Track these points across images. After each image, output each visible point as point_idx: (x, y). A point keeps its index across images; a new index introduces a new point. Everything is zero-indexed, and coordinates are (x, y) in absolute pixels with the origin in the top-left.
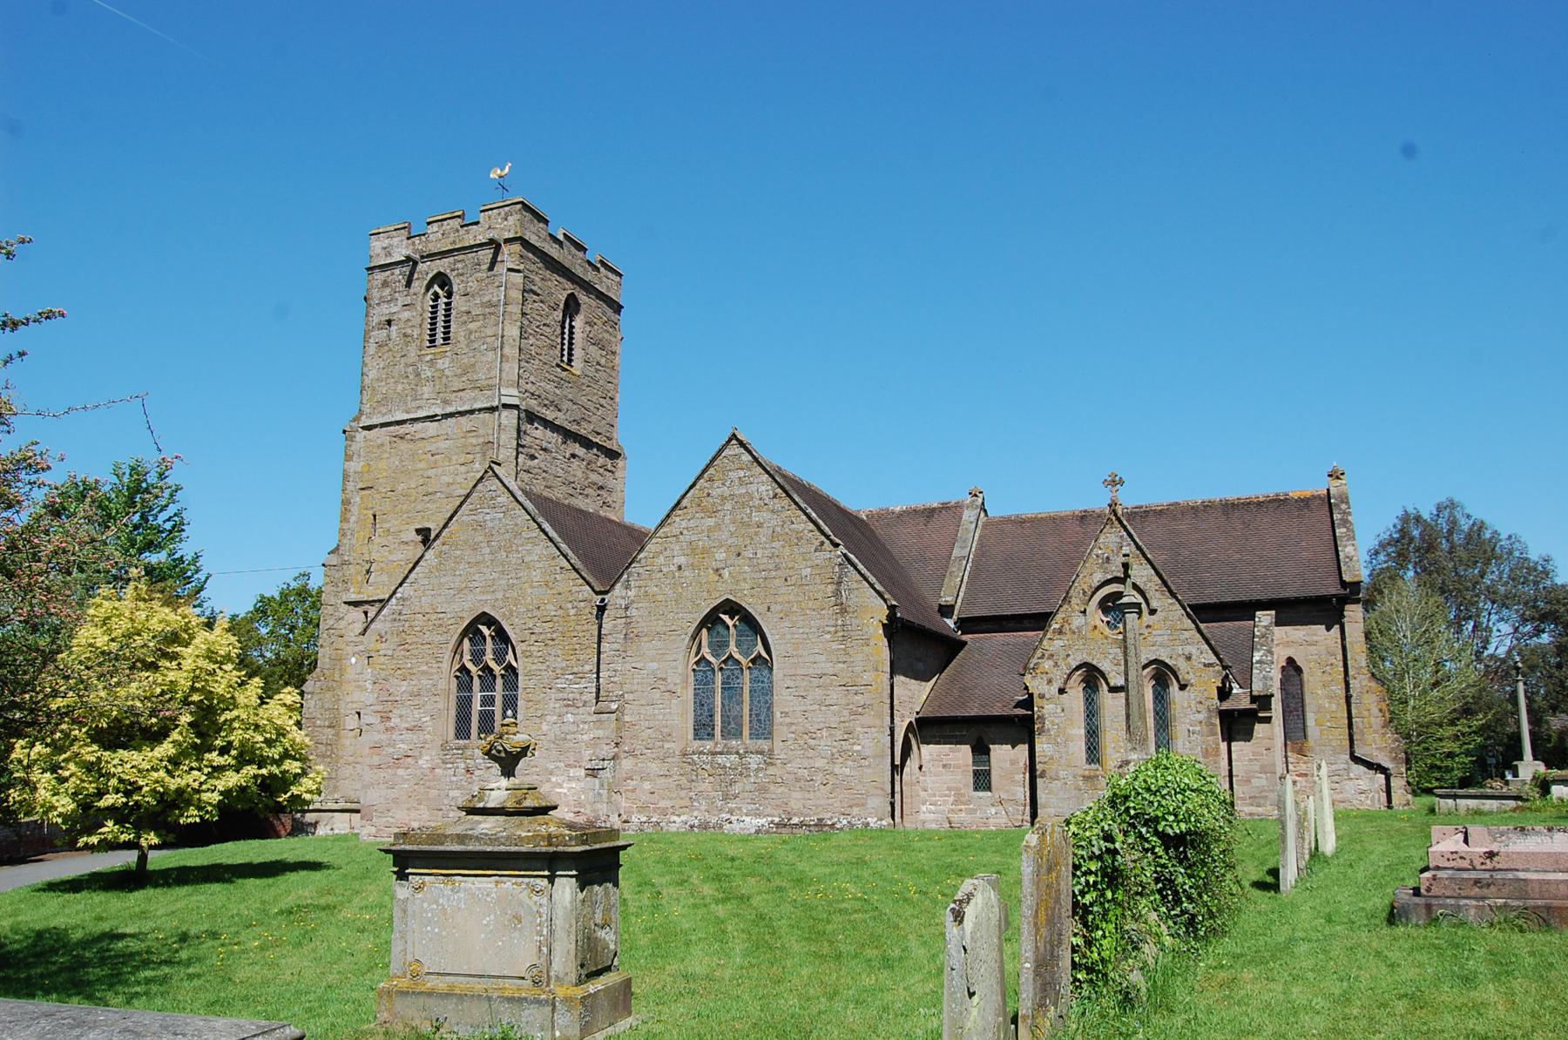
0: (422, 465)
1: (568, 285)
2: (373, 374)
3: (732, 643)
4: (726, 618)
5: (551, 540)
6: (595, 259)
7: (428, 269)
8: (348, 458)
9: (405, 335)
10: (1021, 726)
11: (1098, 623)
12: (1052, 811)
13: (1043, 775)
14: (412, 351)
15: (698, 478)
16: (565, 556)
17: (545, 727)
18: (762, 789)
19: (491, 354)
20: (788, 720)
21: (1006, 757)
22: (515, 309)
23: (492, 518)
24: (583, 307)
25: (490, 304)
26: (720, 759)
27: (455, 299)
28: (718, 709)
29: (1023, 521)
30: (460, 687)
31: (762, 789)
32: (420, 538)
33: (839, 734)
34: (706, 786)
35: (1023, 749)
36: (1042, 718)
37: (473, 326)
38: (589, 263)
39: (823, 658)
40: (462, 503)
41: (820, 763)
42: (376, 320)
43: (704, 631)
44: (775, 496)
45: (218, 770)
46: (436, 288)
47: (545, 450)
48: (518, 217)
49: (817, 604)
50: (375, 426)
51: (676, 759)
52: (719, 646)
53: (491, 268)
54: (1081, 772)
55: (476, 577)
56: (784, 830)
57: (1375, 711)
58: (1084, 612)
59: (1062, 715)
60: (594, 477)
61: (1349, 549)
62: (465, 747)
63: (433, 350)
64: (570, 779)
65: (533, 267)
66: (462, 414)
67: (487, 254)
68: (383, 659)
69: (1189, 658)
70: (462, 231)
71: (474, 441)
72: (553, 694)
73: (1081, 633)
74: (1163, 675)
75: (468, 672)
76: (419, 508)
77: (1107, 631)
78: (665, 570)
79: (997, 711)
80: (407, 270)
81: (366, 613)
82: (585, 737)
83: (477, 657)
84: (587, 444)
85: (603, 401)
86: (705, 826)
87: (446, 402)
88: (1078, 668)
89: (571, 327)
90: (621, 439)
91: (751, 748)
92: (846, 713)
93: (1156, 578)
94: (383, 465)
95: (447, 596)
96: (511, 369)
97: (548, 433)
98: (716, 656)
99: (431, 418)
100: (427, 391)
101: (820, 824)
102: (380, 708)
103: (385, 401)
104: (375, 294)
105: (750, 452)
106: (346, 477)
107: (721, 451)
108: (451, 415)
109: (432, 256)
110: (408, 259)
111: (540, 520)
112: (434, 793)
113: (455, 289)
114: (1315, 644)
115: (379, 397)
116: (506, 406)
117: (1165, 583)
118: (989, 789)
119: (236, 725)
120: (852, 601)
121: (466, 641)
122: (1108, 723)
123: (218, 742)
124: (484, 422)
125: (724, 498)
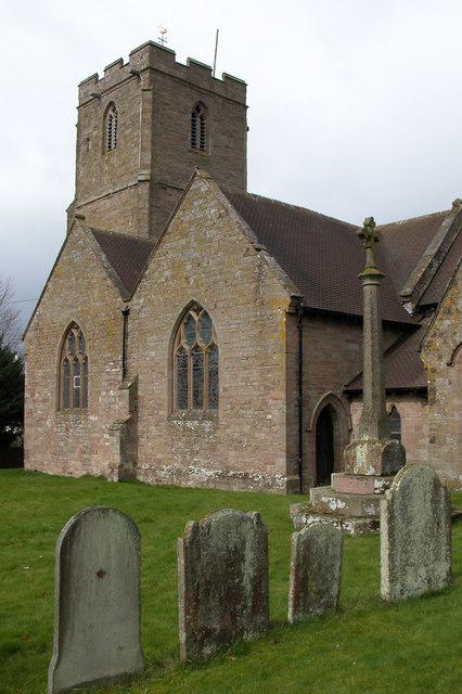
7: (106, 100)
28: (191, 386)
31: (213, 448)
36: (434, 390)
41: (246, 429)
83: (191, 337)
100: (106, 179)
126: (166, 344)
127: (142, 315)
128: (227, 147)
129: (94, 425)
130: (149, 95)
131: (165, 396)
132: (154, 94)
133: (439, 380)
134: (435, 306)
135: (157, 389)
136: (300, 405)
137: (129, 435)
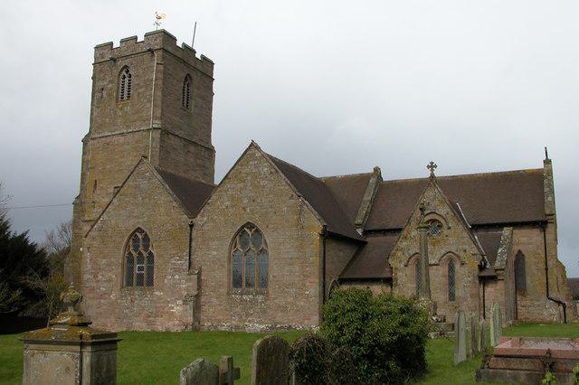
7: (121, 63)
14: (114, 103)
23: (144, 184)
31: (264, 312)
36: (396, 279)
37: (140, 91)
60: (199, 162)
83: (136, 248)
86: (237, 327)
126: (226, 248)
127: (205, 228)
130: (161, 67)
131: (225, 280)
132: (165, 67)
133: (399, 274)
134: (399, 230)
135: (218, 276)
136: (324, 286)
137: (197, 303)
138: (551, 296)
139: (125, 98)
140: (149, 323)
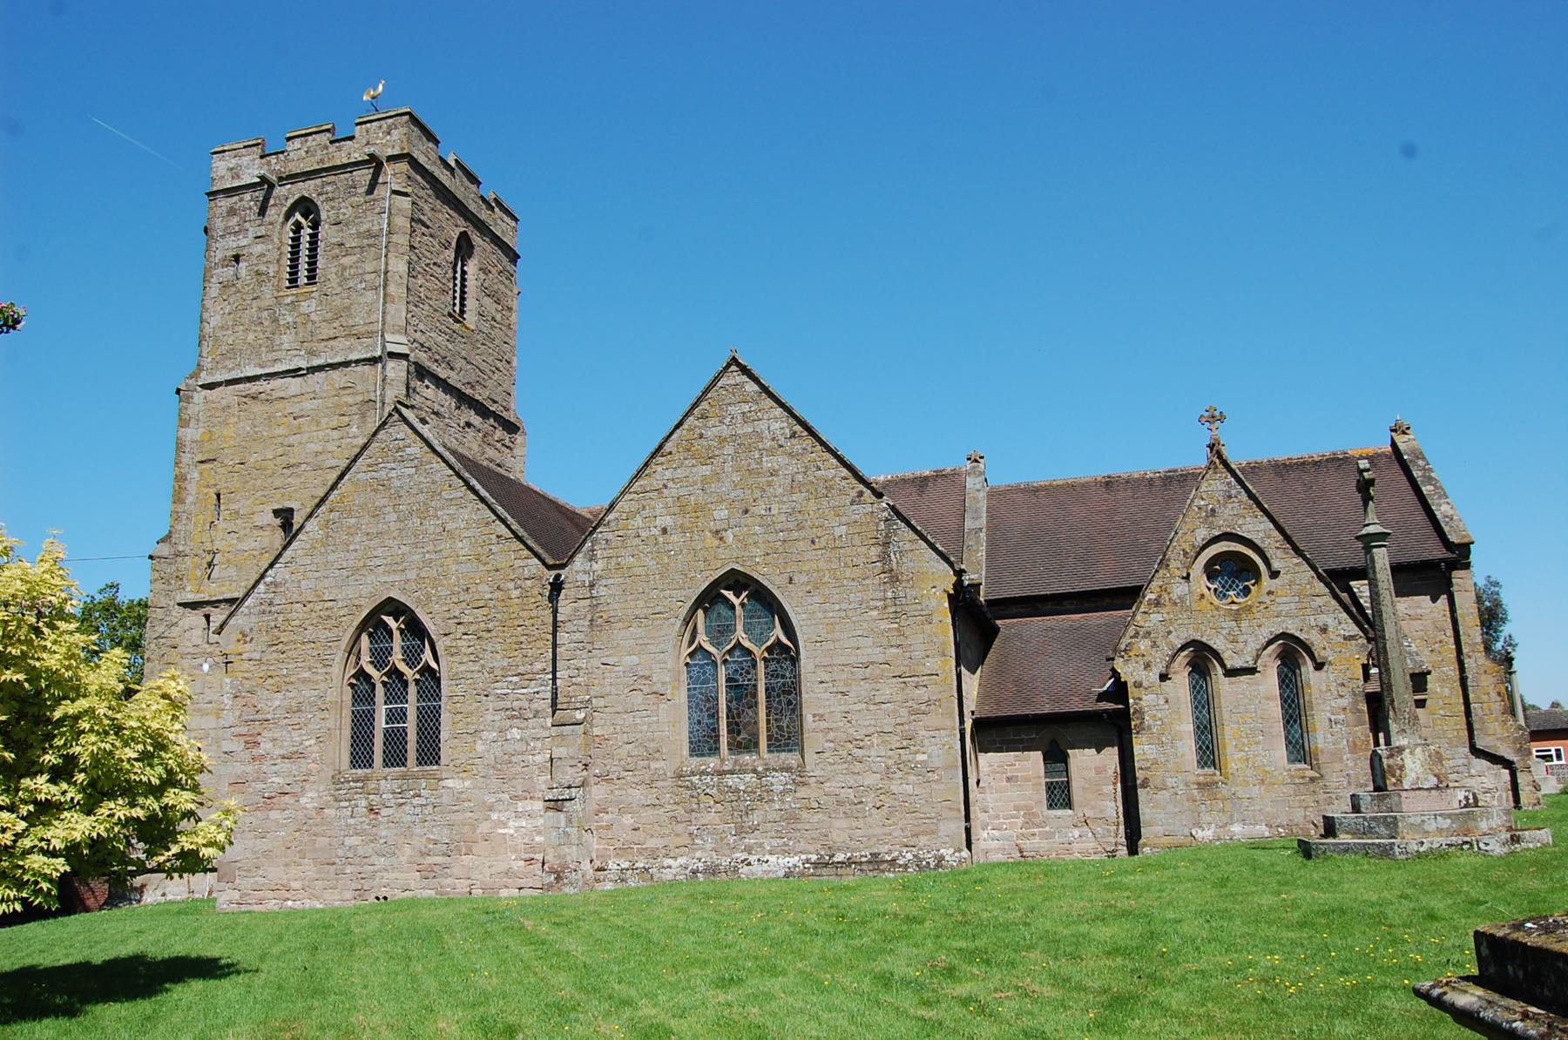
0: (281, 431)
1: (461, 221)
2: (215, 321)
3: (740, 627)
4: (729, 594)
5: (483, 500)
6: (490, 196)
7: (288, 194)
8: (184, 423)
9: (258, 273)
10: (1112, 722)
11: (1205, 591)
12: (1159, 829)
13: (1145, 784)
14: (268, 293)
15: (687, 415)
16: (504, 521)
17: (480, 747)
18: (792, 818)
19: (370, 295)
20: (823, 725)
21: (1092, 767)
22: (401, 240)
23: (400, 475)
24: (477, 250)
25: (369, 234)
26: (731, 780)
27: (323, 230)
28: (723, 714)
29: (1036, 490)
30: (356, 699)
31: (792, 818)
32: (278, 521)
33: (895, 741)
34: (711, 817)
35: (1111, 755)
36: (1139, 712)
37: (346, 261)
38: (482, 198)
39: (869, 641)
40: (357, 457)
41: (871, 780)
42: (220, 255)
43: (700, 612)
44: (793, 435)
45: (46, 810)
46: (298, 216)
47: (436, 414)
48: (405, 130)
49: (857, 572)
50: (219, 384)
51: (669, 782)
52: (721, 632)
53: (370, 191)
54: (1194, 779)
55: (379, 552)
56: (825, 871)
57: (1493, 695)
58: (1187, 578)
59: (1164, 708)
61: (1444, 508)
62: (366, 779)
63: (294, 291)
64: (518, 815)
65: (422, 193)
66: (333, 366)
67: (364, 176)
68: (247, 665)
69: (1324, 630)
70: (332, 148)
71: (350, 400)
72: (491, 703)
73: (1181, 604)
74: (1292, 653)
75: (368, 677)
76: (278, 483)
77: (1216, 602)
78: (644, 534)
79: (1076, 706)
80: (260, 195)
81: (207, 617)
82: (538, 758)
83: (380, 658)
84: (483, 412)
85: (499, 365)
86: (712, 870)
87: (311, 353)
88: (1183, 648)
89: (464, 273)
90: (517, 411)
91: (772, 764)
92: (904, 712)
93: (1276, 534)
94: (229, 431)
95: (338, 578)
96: (398, 312)
97: (441, 394)
98: (718, 645)
99: (294, 373)
101: (875, 860)
102: (244, 730)
103: (232, 352)
104: (219, 224)
105: (756, 380)
106: (180, 446)
107: (716, 379)
108: (320, 368)
109: (293, 178)
110: (264, 179)
111: (467, 475)
112: (322, 841)
113: (323, 216)
114: (1419, 618)
115: (224, 349)
116: (392, 355)
117: (1288, 539)
118: (1068, 804)
119: (84, 725)
120: (906, 566)
121: (365, 638)
122: (1226, 715)
123: (50, 758)
124: (364, 378)
125: (722, 440)
128: (493, 319)
129: (459, 797)
138: (1480, 744)
139: (303, 280)
140: (427, 873)
